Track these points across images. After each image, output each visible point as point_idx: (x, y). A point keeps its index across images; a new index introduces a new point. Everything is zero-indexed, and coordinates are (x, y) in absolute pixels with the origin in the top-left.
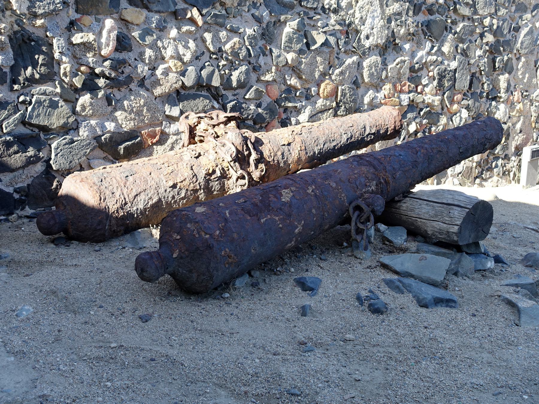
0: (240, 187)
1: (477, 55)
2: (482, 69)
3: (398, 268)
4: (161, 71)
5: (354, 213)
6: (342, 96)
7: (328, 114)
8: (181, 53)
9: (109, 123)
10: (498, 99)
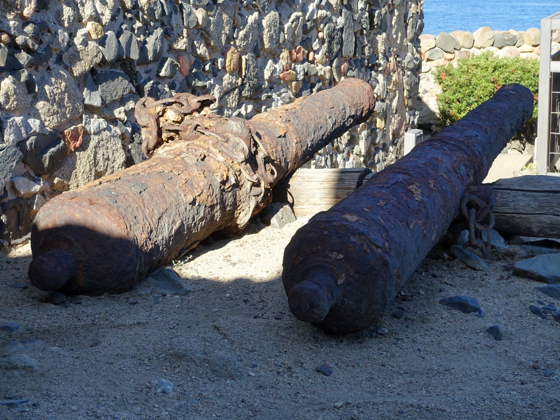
0: (254, 198)
1: (359, 8)
2: (364, 26)
3: (543, 273)
4: (81, 39)
5: (469, 213)
6: (246, 69)
7: (234, 95)
8: (100, 12)
9: (32, 120)
10: (376, 68)
